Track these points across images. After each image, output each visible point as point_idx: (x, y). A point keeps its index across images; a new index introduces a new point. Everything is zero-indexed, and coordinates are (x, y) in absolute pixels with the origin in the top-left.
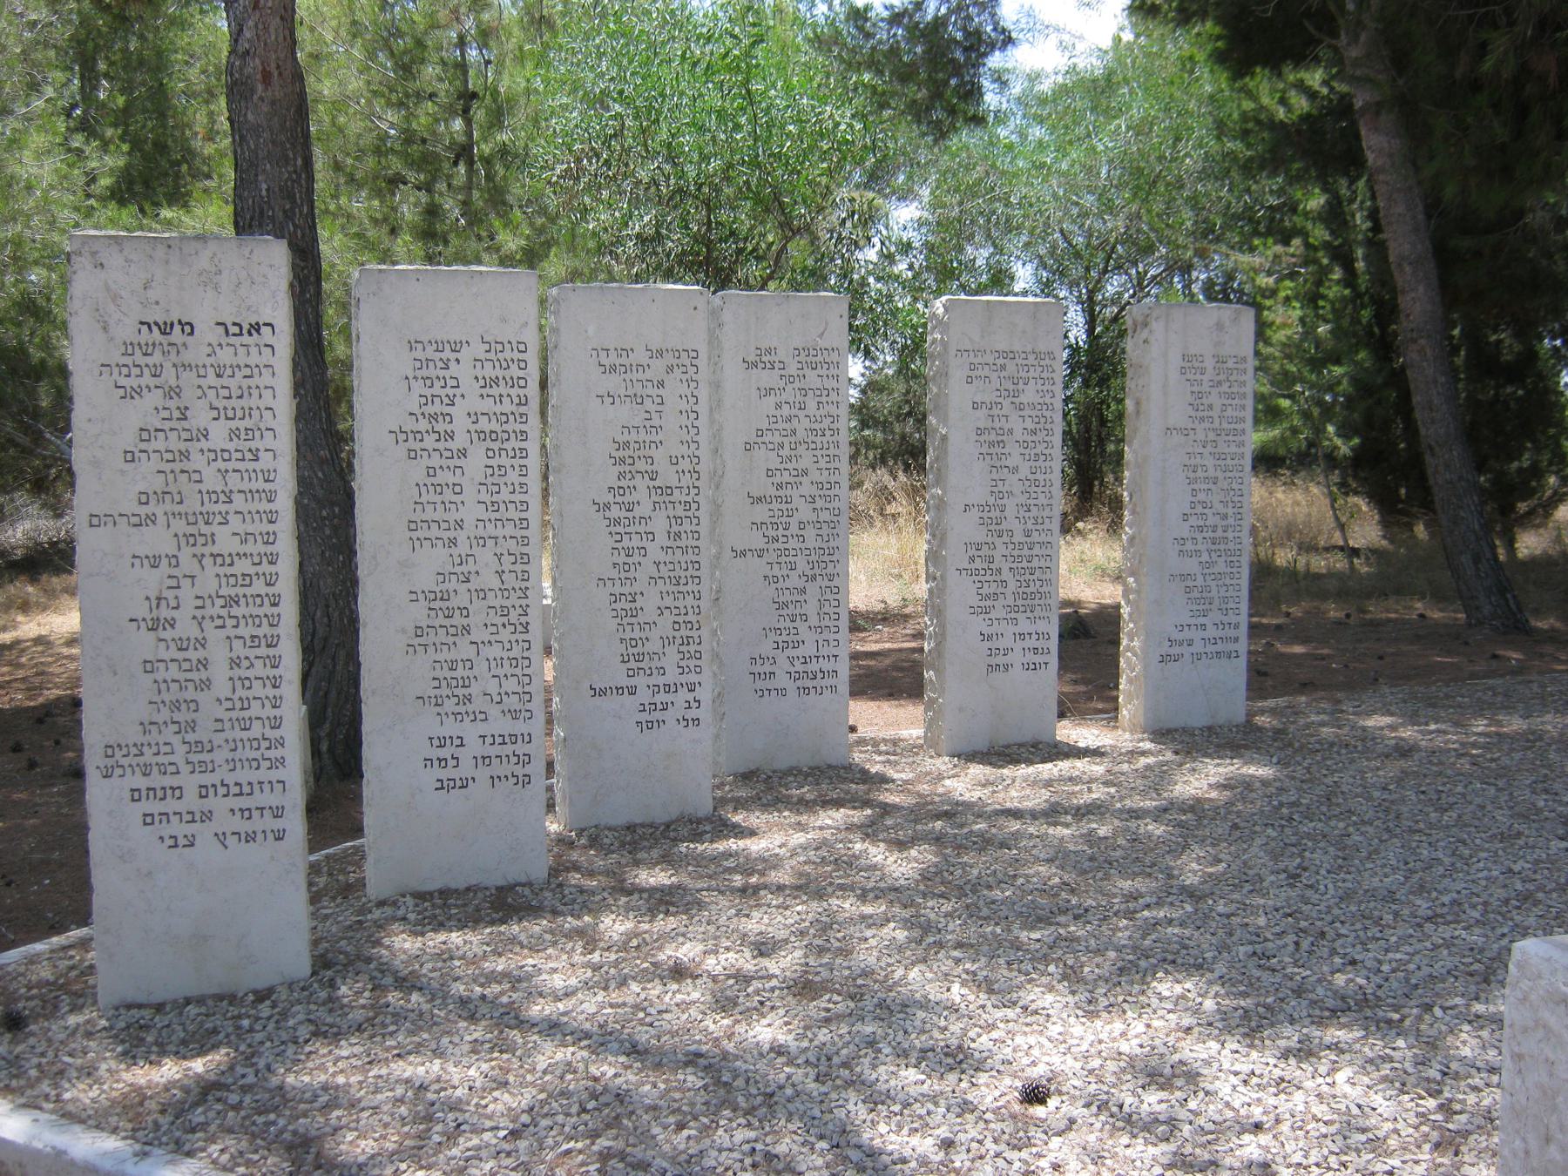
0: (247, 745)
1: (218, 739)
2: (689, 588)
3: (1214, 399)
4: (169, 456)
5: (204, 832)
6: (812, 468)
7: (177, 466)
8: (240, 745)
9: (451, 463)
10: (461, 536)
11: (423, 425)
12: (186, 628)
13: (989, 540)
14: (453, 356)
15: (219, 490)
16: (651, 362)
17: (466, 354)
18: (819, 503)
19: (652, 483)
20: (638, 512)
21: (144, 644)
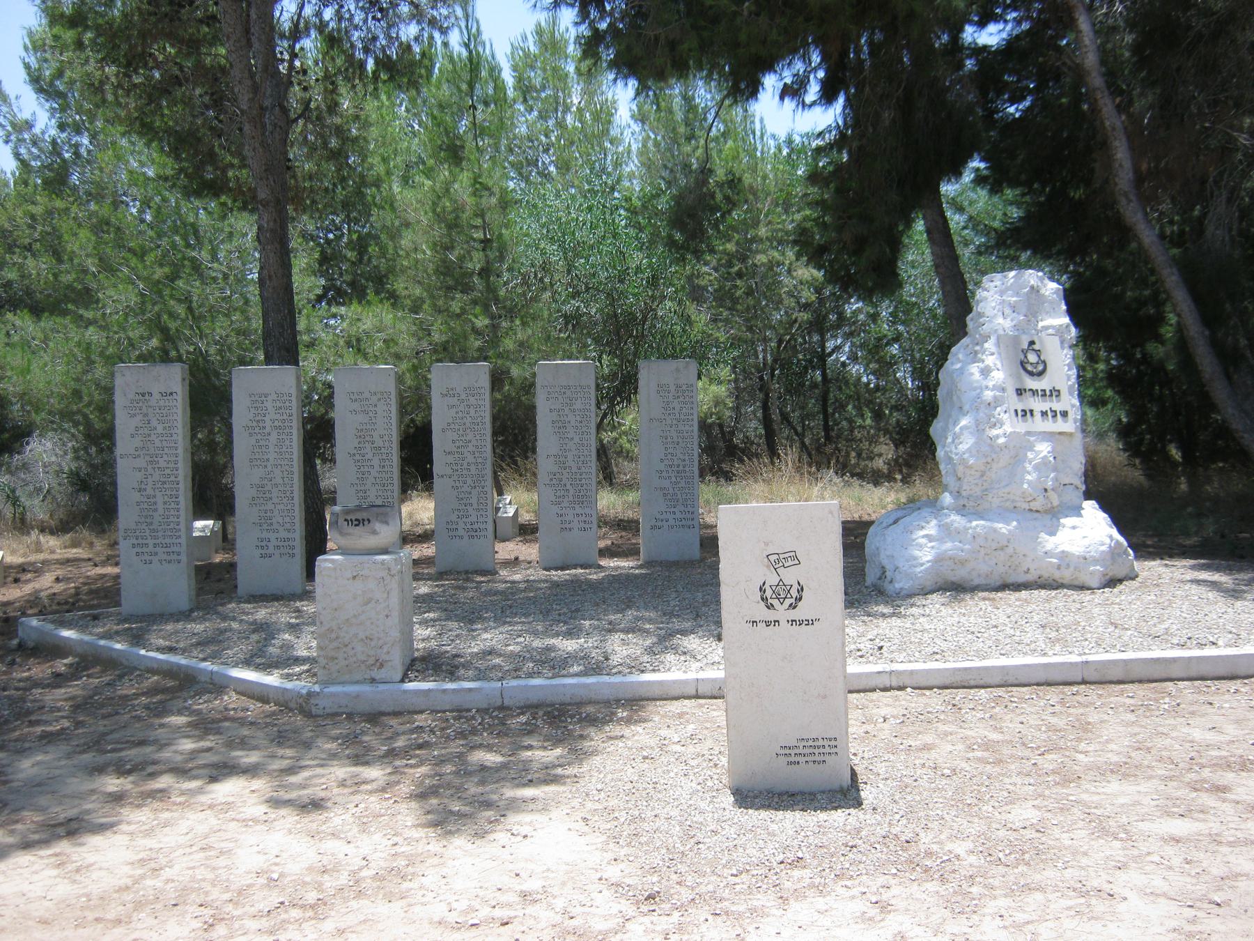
3: (676, 404)
5: (155, 559)
10: (269, 464)
11: (255, 424)
12: (150, 491)
17: (270, 398)
18: (477, 455)
20: (367, 457)
21: (136, 496)
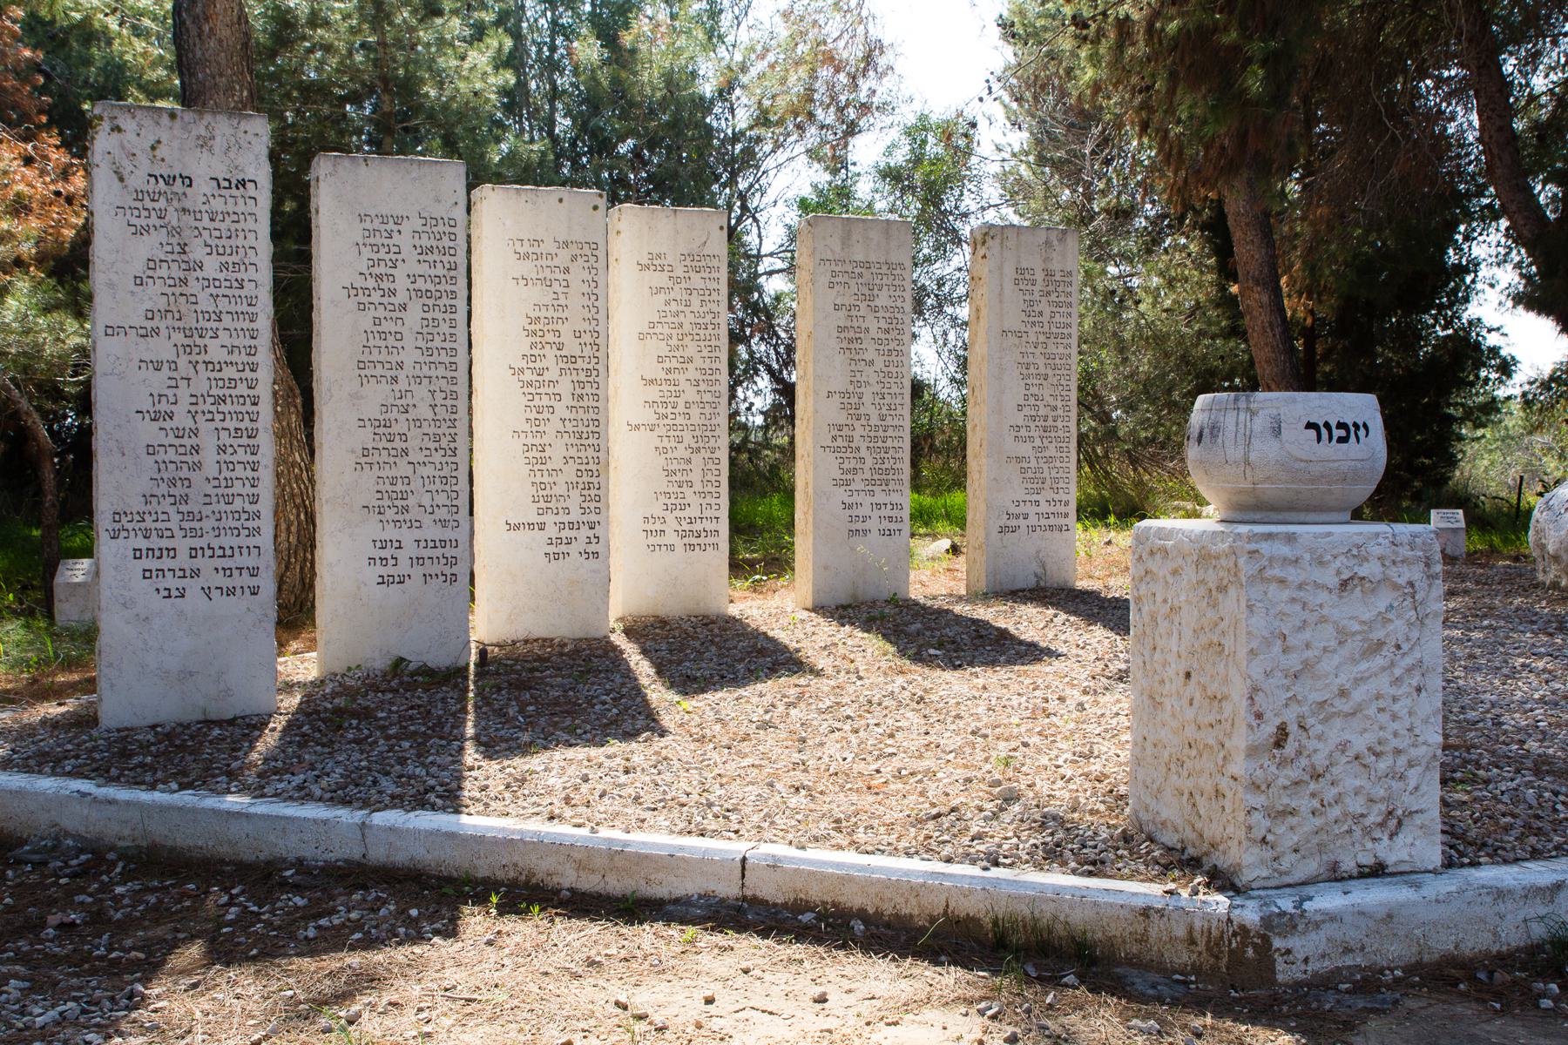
0: (230, 516)
1: (207, 510)
2: (590, 441)
3: (1043, 306)
4: (171, 282)
6: (697, 357)
7: (178, 290)
8: (224, 516)
9: (394, 315)
10: (402, 375)
11: (371, 283)
12: (182, 420)
13: (849, 422)
14: (396, 228)
15: (211, 310)
16: (558, 251)
17: (406, 227)
18: (703, 387)
19: (559, 353)
20: (547, 376)
21: (149, 432)
